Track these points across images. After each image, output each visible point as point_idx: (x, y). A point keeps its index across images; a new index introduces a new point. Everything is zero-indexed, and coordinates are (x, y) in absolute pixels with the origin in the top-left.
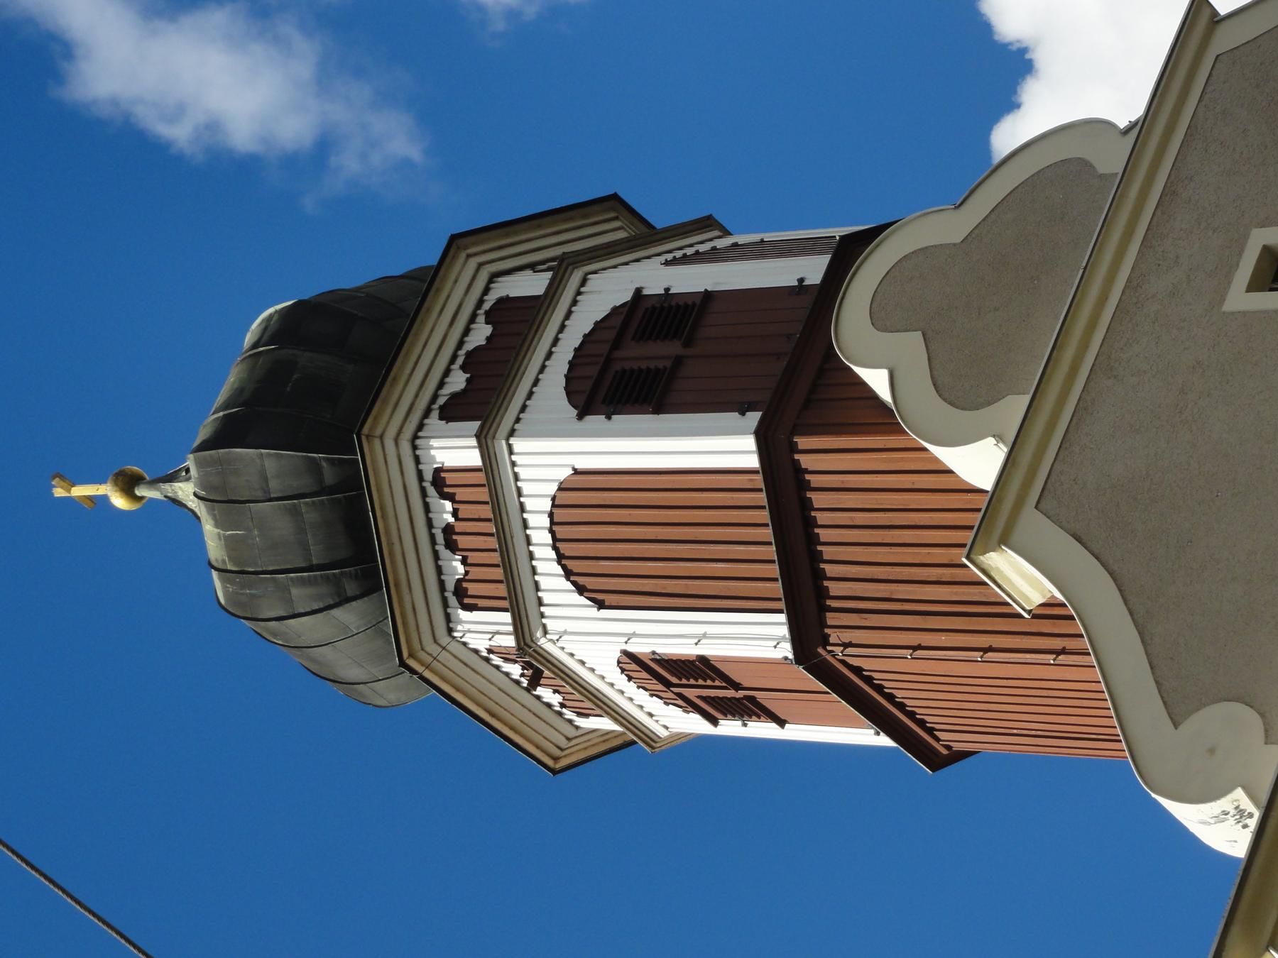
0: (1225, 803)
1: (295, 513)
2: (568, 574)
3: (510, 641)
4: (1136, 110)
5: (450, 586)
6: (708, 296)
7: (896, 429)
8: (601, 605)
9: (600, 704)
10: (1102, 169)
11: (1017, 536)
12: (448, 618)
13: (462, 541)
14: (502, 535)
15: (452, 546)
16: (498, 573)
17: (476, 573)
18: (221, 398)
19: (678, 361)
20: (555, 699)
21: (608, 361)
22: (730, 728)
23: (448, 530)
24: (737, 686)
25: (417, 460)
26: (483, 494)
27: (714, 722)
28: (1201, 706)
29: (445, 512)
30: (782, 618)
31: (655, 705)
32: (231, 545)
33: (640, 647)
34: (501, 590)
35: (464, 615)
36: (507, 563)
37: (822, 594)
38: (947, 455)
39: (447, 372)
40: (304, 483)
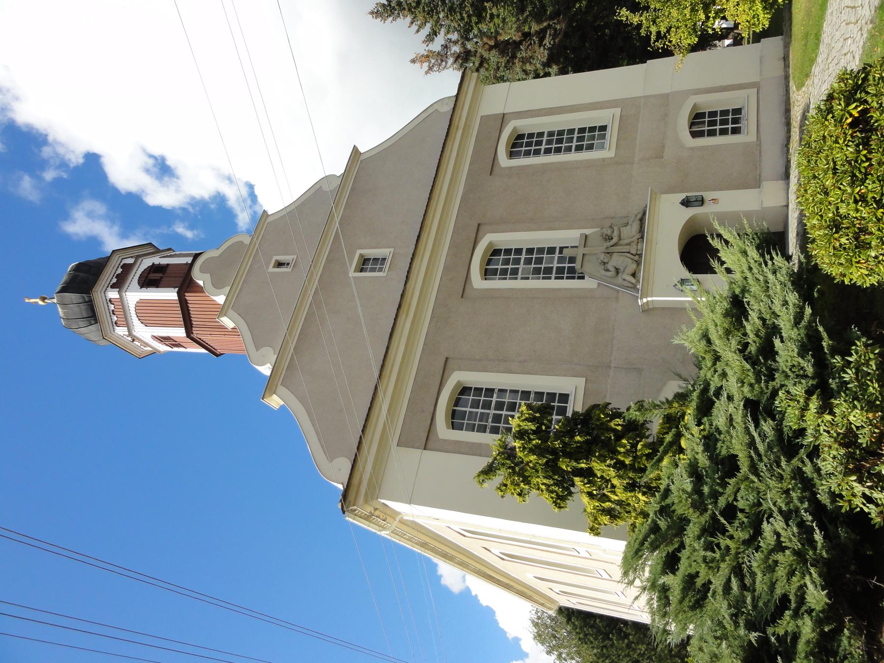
1: (79, 306)
2: (139, 320)
3: (127, 333)
5: (114, 322)
6: (168, 265)
7: (203, 292)
8: (146, 326)
9: (147, 345)
10: (246, 243)
11: (228, 314)
12: (114, 329)
13: (116, 313)
14: (124, 312)
15: (114, 314)
16: (124, 319)
17: (119, 319)
18: (62, 282)
20: (139, 344)
21: (147, 277)
22: (176, 349)
23: (113, 311)
24: (176, 342)
25: (105, 296)
26: (120, 304)
27: (172, 348)
28: (261, 348)
29: (112, 307)
30: (184, 329)
31: (160, 345)
32: (65, 313)
33: (156, 334)
34: (125, 323)
35: (117, 328)
36: (126, 317)
37: (192, 324)
38: (214, 298)
39: (112, 278)
40: (81, 301)
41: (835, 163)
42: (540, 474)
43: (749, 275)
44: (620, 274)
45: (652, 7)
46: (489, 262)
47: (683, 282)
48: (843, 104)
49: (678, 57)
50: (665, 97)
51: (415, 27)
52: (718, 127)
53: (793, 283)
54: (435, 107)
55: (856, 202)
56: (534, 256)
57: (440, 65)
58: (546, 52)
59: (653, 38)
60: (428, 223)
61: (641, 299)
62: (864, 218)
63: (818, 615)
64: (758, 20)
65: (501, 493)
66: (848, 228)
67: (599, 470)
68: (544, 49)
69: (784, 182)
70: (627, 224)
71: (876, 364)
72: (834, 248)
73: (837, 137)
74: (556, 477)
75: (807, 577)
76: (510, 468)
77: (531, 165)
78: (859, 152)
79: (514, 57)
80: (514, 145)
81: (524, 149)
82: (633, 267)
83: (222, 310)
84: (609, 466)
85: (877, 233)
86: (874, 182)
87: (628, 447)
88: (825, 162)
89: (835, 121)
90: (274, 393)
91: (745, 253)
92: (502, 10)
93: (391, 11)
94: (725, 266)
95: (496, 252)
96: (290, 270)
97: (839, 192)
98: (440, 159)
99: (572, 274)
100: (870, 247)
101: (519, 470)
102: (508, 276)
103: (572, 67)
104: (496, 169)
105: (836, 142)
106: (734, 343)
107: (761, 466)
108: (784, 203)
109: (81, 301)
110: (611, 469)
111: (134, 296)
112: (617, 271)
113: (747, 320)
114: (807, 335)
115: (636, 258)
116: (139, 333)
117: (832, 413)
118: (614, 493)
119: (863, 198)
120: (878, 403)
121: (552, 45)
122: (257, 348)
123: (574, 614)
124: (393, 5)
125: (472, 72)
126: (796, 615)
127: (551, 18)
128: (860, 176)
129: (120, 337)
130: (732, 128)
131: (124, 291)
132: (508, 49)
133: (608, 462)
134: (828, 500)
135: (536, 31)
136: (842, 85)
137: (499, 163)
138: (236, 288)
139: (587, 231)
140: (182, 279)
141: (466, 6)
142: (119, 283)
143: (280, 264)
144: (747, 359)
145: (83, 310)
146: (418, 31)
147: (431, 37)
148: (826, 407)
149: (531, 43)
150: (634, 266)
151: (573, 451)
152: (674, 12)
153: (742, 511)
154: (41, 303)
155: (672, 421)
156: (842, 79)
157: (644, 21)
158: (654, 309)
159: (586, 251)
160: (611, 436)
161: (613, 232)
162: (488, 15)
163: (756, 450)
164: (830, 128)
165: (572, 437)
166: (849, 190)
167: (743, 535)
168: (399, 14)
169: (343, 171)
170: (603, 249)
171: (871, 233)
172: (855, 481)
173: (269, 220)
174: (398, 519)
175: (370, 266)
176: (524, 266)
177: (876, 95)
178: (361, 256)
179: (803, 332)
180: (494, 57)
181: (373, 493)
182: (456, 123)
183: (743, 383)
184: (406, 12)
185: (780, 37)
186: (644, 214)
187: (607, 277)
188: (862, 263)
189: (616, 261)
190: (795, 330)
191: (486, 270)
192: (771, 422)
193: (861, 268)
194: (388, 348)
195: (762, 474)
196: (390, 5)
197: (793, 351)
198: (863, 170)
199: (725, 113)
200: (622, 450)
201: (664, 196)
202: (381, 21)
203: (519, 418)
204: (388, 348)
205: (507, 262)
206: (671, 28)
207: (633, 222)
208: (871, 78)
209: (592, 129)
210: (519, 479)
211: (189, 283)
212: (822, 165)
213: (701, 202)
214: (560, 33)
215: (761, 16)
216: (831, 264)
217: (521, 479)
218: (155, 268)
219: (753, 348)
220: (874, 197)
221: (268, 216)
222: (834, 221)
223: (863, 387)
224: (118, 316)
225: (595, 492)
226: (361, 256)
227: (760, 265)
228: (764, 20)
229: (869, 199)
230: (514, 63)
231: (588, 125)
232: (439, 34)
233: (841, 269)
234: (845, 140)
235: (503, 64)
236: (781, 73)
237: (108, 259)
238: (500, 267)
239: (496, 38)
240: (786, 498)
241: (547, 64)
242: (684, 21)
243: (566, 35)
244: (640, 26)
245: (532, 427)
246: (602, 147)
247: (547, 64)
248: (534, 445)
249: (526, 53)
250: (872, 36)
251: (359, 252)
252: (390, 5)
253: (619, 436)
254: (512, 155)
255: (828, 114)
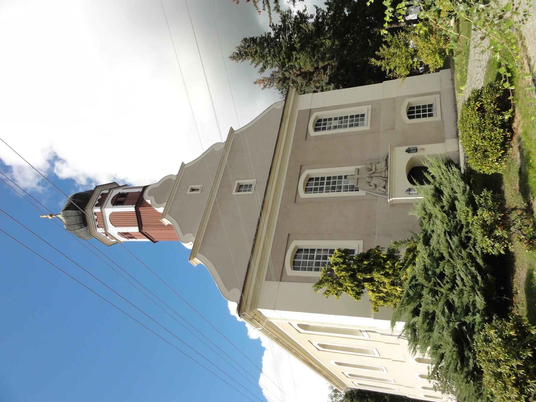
0: (190, 243)
1: (76, 218)
2: (111, 223)
4: (177, 173)
5: (96, 225)
6: (128, 193)
8: (115, 227)
14: (103, 219)
15: (96, 221)
19: (125, 200)
21: (116, 200)
22: (130, 240)
23: (96, 219)
24: (131, 235)
26: (101, 215)
27: (128, 239)
29: (96, 217)
31: (121, 238)
33: (120, 231)
35: (98, 229)
37: (142, 224)
38: (157, 209)
40: (77, 214)
41: (473, 125)
42: (347, 281)
43: (442, 176)
44: (377, 187)
45: (386, 58)
46: (307, 185)
47: (409, 190)
48: (474, 102)
49: (399, 80)
50: (394, 99)
51: (254, 65)
52: (421, 114)
53: (461, 178)
54: (274, 106)
55: (482, 139)
56: (331, 181)
57: (270, 85)
58: (328, 77)
59: (388, 72)
60: (274, 165)
61: (389, 199)
62: (485, 146)
63: (482, 313)
64: (438, 63)
65: (326, 296)
66: (479, 150)
67: (376, 278)
68: (327, 76)
69: (456, 139)
70: (379, 163)
71: (491, 196)
72: (476, 159)
73: (473, 115)
74: (355, 282)
75: (476, 296)
76: (330, 282)
77: (327, 135)
78: (481, 120)
79: (310, 79)
80: (316, 125)
81: (322, 127)
82: (383, 183)
83: (163, 215)
84: (382, 275)
85: (491, 151)
86: (488, 131)
87: (391, 265)
88: (469, 125)
89: (471, 108)
90: (195, 257)
91: (440, 167)
92: (301, 56)
93: (241, 56)
94: (431, 174)
95: (311, 179)
96: (200, 192)
97: (475, 136)
98: (279, 133)
99: (353, 188)
100: (489, 157)
101: (336, 282)
102: (318, 191)
103: (341, 85)
104: (308, 137)
105: (472, 117)
106: (438, 207)
107: (454, 255)
108: (457, 150)
109: (76, 214)
110: (383, 276)
111: (109, 210)
112: (376, 186)
113: (443, 196)
114: (468, 198)
115: (385, 179)
116: (111, 231)
117: (477, 215)
118: (385, 288)
119: (484, 138)
120: (492, 208)
121: (331, 74)
122: (184, 235)
123: (354, 397)
124: (242, 53)
125: (293, 88)
126: (474, 314)
127: (330, 59)
128: (482, 129)
129: (99, 234)
130: (428, 114)
131: (103, 207)
132: (307, 76)
133: (381, 272)
134: (482, 263)
135: (322, 67)
136: (473, 95)
137: (310, 134)
138: (170, 203)
139: (359, 167)
140: (137, 200)
141: (282, 53)
142: (101, 203)
143: (193, 190)
144: (444, 212)
145: (78, 220)
146: (256, 66)
147: (263, 70)
148: (475, 213)
149: (319, 73)
150: (384, 183)
151: (363, 269)
152: (398, 60)
153: (447, 276)
154: (50, 217)
155: (412, 250)
156: (473, 93)
157: (383, 64)
158: (396, 204)
159: (359, 176)
160: (381, 261)
161: (372, 166)
162: (294, 58)
163: (451, 248)
164: (470, 111)
165: (362, 262)
166: (479, 135)
167: (448, 286)
168: (245, 58)
169: (226, 140)
170: (368, 175)
171: (489, 151)
172: (487, 238)
173: (186, 167)
174: (266, 321)
175: (243, 189)
176: (327, 186)
177: (485, 99)
178: (238, 184)
179: (467, 196)
180: (299, 80)
181: (254, 305)
182: (286, 114)
183: (443, 223)
184: (249, 57)
185: (449, 69)
186: (387, 157)
187: (370, 189)
188: (487, 164)
189: (375, 181)
190: (464, 196)
191: (306, 188)
192: (457, 237)
193: (487, 166)
194: (257, 230)
195: (454, 258)
196: (240, 53)
197: (463, 204)
198: (483, 127)
199: (424, 106)
200: (387, 267)
201: (397, 148)
202: (236, 61)
203: (334, 256)
204: (257, 230)
205: (316, 184)
206: (396, 67)
207: (382, 161)
208: (483, 92)
209: (357, 116)
210: (336, 286)
211: (142, 201)
212: (468, 125)
213: (416, 150)
214: (335, 67)
215: (439, 61)
216: (475, 165)
217: (337, 285)
218: (120, 195)
219: (446, 208)
220: (488, 137)
221: (185, 165)
222: (475, 148)
223: (487, 203)
224: (99, 222)
225: (375, 289)
226: (238, 184)
227: (447, 171)
228: (441, 63)
229: (486, 138)
230: (310, 83)
231: (355, 114)
232: (267, 68)
233: (479, 167)
234: (475, 116)
235: (305, 84)
236: (450, 87)
237: (92, 192)
238: (313, 187)
239: (300, 71)
240: (466, 267)
241: (328, 84)
242: (402, 64)
243: (338, 68)
244: (381, 66)
245: (341, 260)
246: (363, 125)
247: (328, 84)
248: (343, 268)
249: (317, 78)
250: (487, 74)
251: (237, 182)
252: (240, 53)
253: (385, 261)
254: (316, 130)
255: (469, 106)
